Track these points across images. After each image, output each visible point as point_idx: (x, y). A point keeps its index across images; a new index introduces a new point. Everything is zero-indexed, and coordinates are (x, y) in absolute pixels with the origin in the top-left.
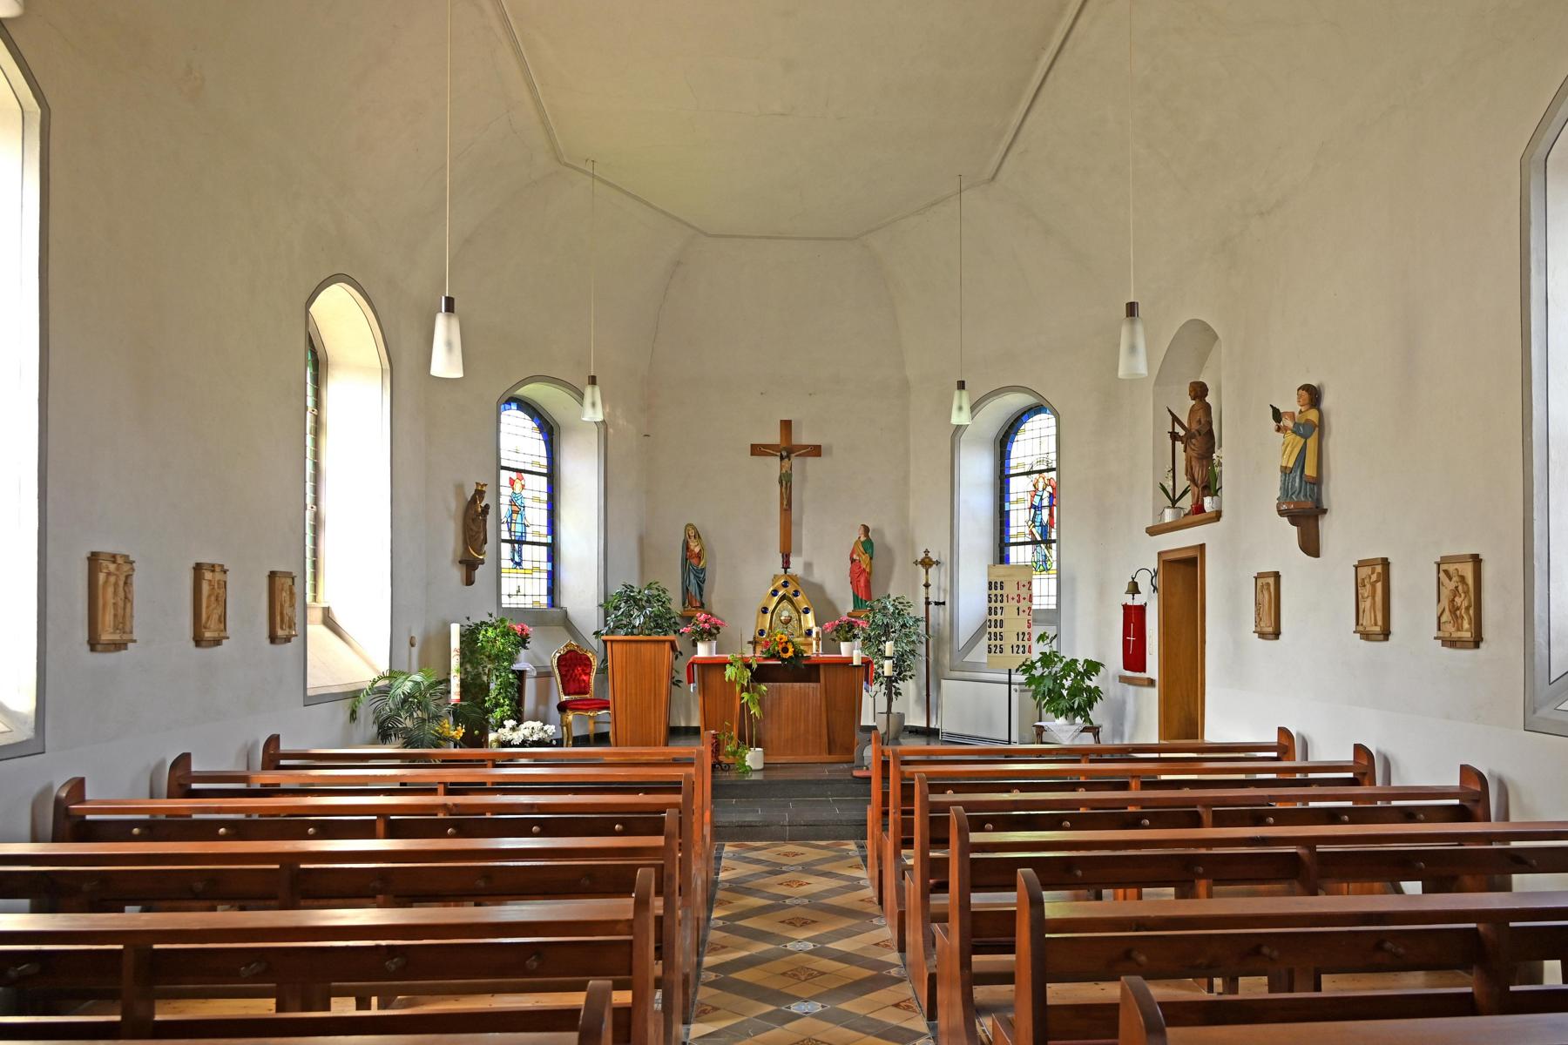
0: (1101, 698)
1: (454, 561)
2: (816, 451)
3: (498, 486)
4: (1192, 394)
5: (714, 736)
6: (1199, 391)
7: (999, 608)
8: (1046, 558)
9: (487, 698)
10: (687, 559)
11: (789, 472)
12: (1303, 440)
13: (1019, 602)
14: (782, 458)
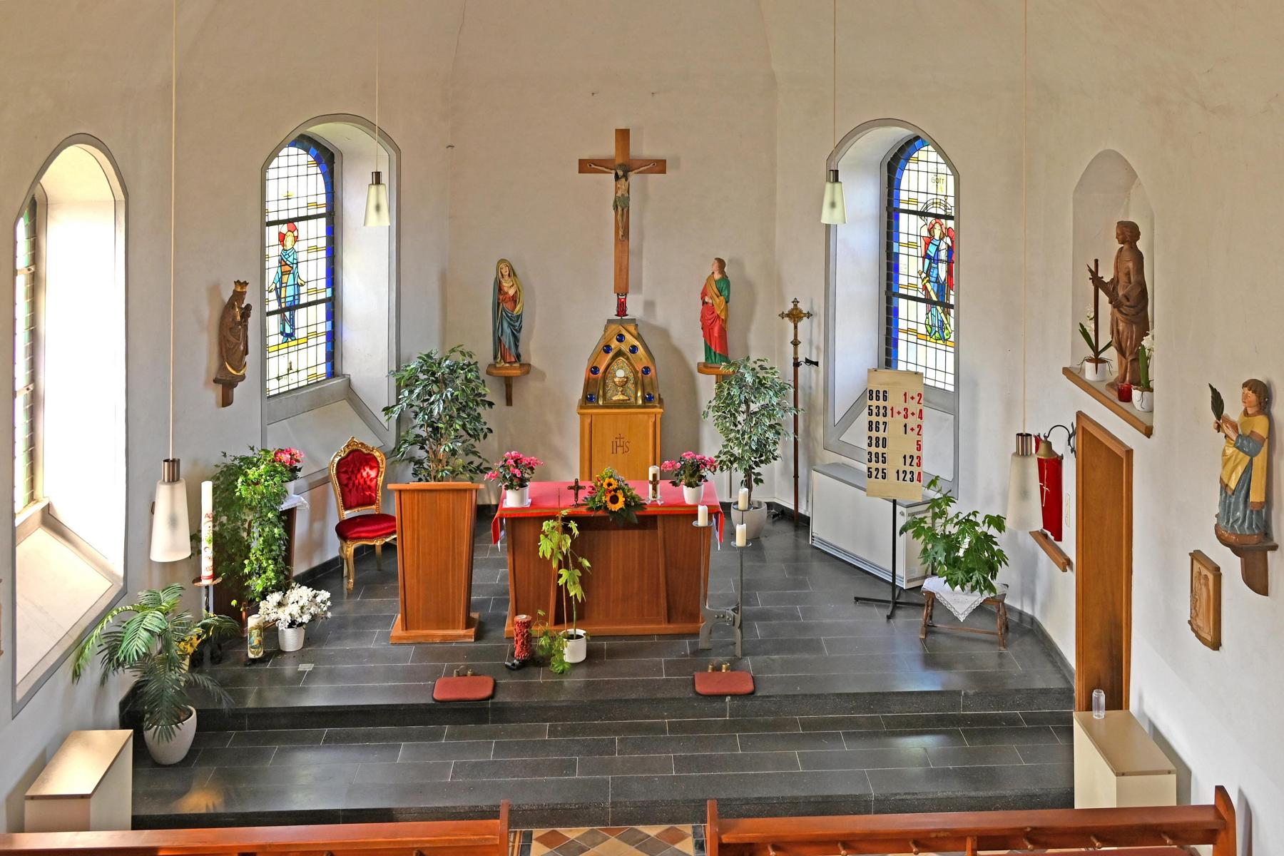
0: (1006, 563)
1: (206, 384)
2: (659, 166)
3: (263, 247)
4: (1121, 237)
5: (527, 625)
6: (1129, 233)
7: (881, 423)
8: (942, 327)
9: (246, 562)
10: (499, 304)
11: (626, 195)
12: (1249, 458)
13: (906, 417)
14: (617, 177)
